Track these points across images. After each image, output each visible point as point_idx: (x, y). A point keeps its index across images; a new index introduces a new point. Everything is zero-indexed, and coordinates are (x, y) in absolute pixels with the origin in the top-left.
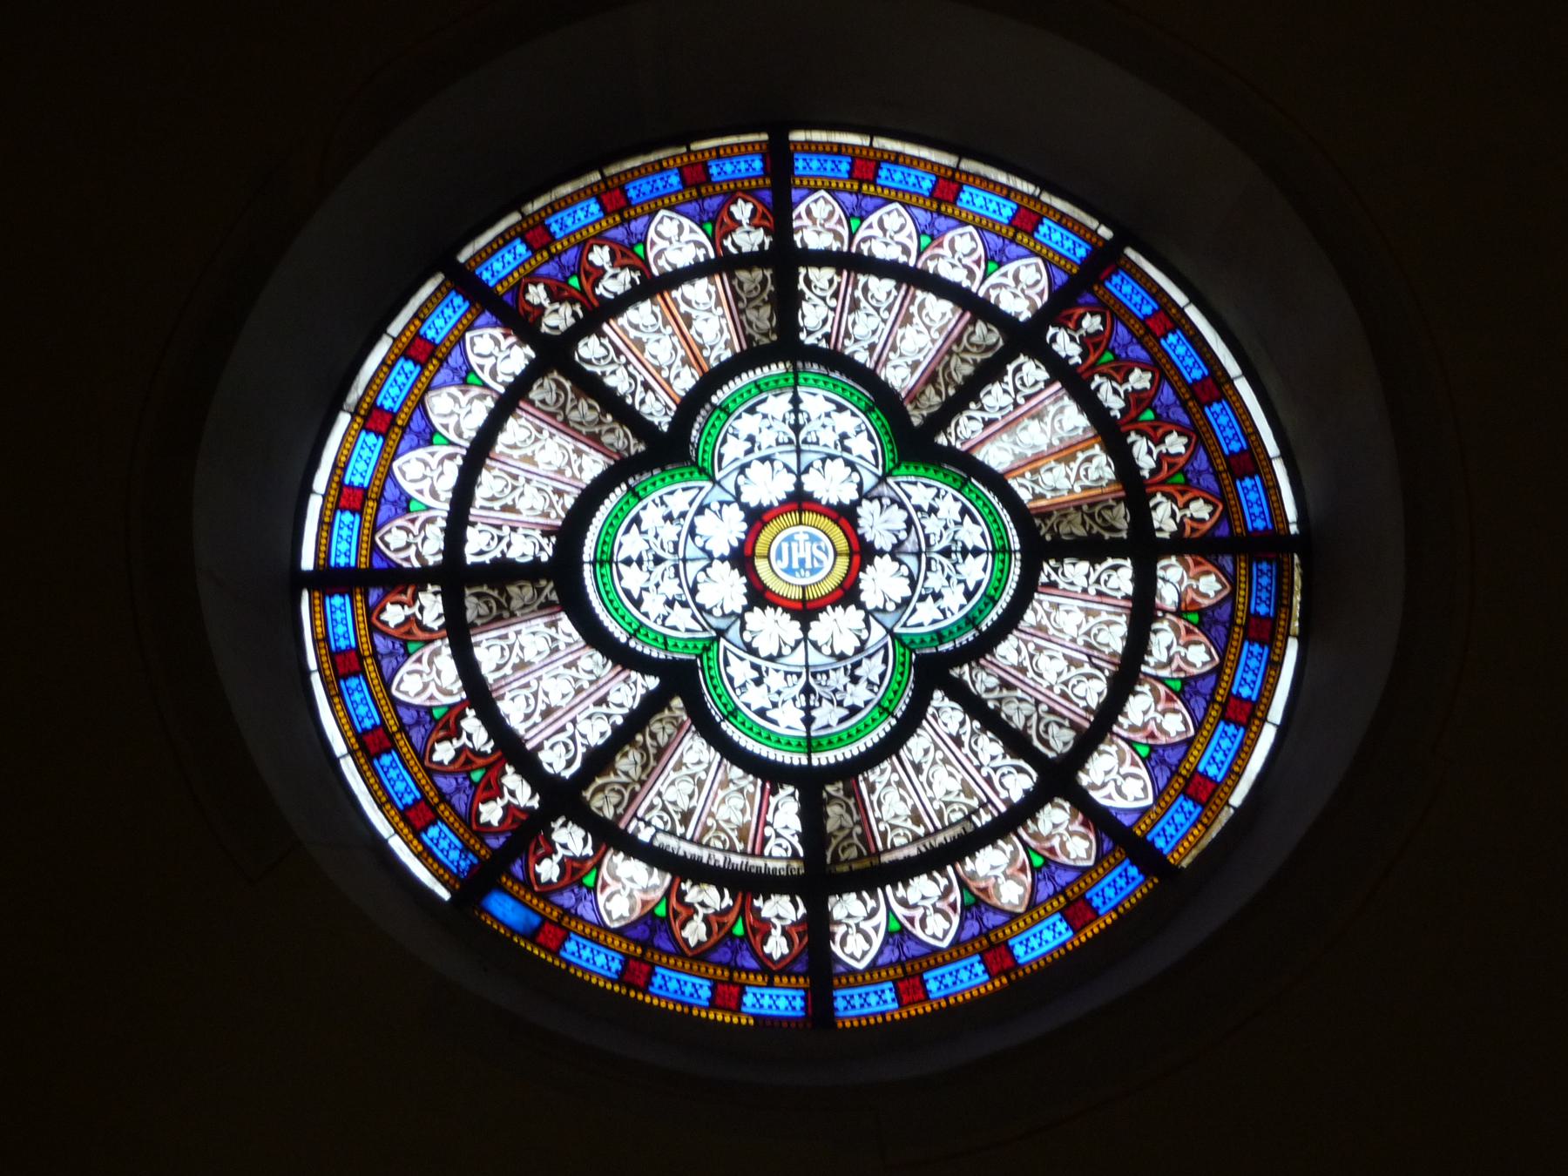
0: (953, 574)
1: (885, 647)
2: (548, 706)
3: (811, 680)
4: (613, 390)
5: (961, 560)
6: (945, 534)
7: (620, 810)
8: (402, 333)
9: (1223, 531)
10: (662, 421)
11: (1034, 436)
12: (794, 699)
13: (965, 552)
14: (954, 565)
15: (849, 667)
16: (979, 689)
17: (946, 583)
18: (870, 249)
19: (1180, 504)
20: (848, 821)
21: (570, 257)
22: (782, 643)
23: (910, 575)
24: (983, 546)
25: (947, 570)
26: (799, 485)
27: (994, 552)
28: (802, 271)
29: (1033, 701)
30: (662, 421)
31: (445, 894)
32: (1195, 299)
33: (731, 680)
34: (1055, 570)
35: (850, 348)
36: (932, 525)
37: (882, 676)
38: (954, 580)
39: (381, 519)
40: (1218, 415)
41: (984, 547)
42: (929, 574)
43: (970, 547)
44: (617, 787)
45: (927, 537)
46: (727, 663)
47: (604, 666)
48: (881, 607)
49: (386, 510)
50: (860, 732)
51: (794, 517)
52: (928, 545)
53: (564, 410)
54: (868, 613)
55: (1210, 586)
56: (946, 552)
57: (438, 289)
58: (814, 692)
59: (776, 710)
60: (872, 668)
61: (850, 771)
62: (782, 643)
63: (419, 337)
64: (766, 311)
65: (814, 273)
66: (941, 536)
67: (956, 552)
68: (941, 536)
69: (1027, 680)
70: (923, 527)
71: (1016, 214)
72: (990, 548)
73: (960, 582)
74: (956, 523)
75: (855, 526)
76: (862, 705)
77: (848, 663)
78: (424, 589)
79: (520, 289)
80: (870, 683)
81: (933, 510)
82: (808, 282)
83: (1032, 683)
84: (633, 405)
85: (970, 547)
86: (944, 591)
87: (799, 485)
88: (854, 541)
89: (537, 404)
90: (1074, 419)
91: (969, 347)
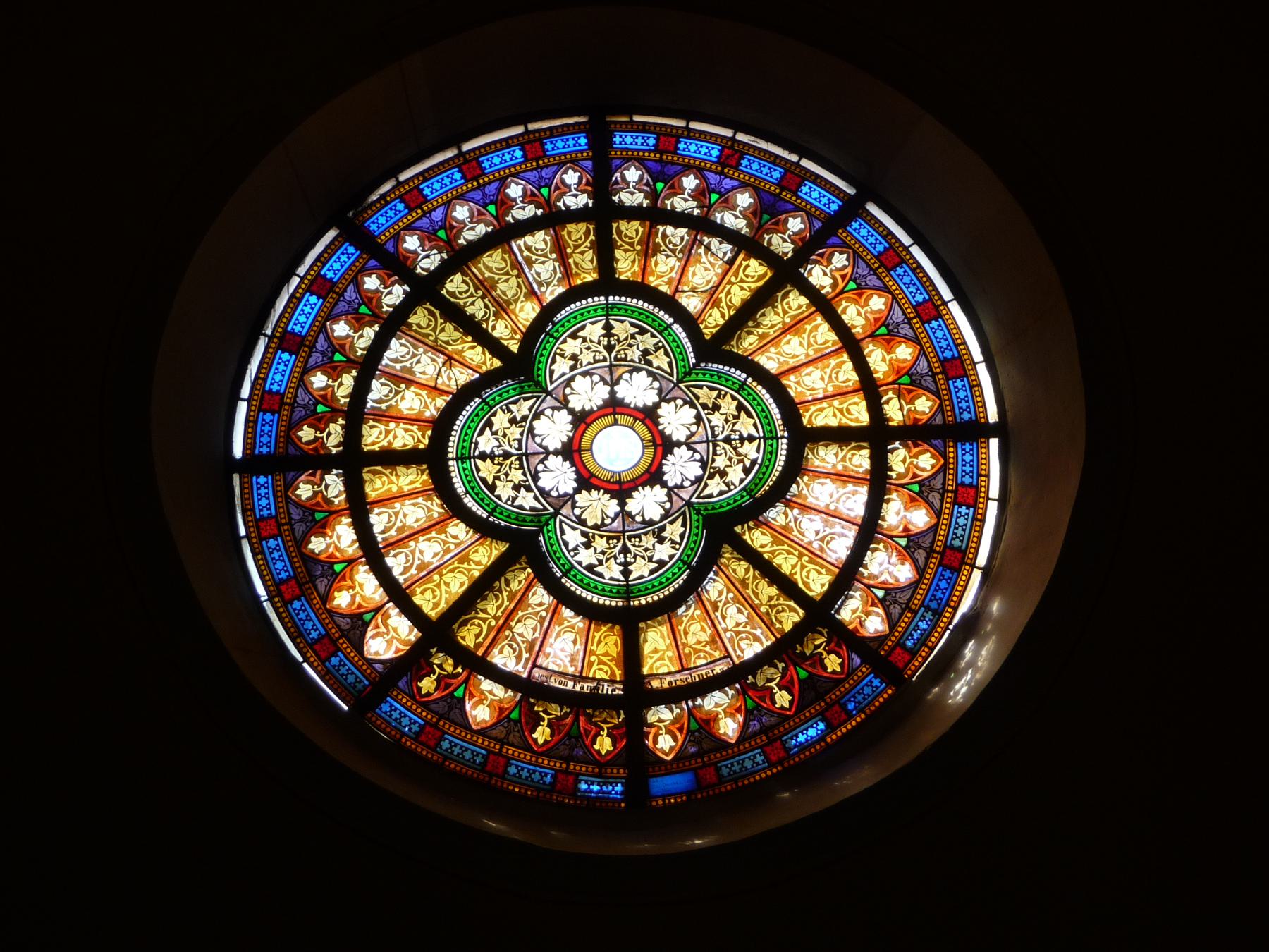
0: (501, 438)
1: (684, 513)
2: (423, 562)
3: (627, 540)
4: (770, 584)
5: (495, 449)
6: (726, 426)
7: (480, 640)
8: (308, 272)
9: (939, 420)
10: (727, 553)
11: (794, 348)
12: (616, 558)
13: (492, 457)
14: (500, 446)
15: (579, 366)
16: (756, 545)
17: (729, 463)
18: (672, 204)
19: (320, 495)
20: (577, 257)
21: (438, 215)
22: (604, 516)
23: (534, 436)
24: (755, 434)
25: (729, 453)
26: (613, 393)
27: (765, 439)
28: (615, 225)
29: (796, 553)
30: (727, 553)
31: (346, 708)
32: (919, 240)
33: (566, 544)
34: (419, 441)
35: (579, 622)
36: (517, 476)
37: (682, 536)
38: (500, 434)
39: (940, 477)
40: (282, 567)
41: (756, 435)
42: (519, 437)
43: (745, 435)
44: (749, 279)
45: (712, 428)
46: (563, 533)
47: (467, 532)
48: (556, 412)
49: (938, 483)
50: (669, 582)
51: (610, 419)
52: (714, 435)
53: (802, 565)
54: (670, 490)
55: (926, 461)
56: (727, 440)
57: (335, 239)
58: (605, 347)
59: (602, 567)
60: (674, 530)
61: (575, 294)
62: (604, 516)
63: (320, 277)
64: (590, 255)
65: (624, 225)
66: (723, 428)
67: (735, 440)
68: (723, 428)
69: (792, 537)
70: (710, 421)
71: (783, 176)
72: (762, 435)
73: (739, 462)
74: (499, 479)
75: (657, 424)
76: (667, 559)
77: (580, 370)
78: (329, 472)
79: (398, 239)
80: (673, 542)
81: (516, 488)
82: (619, 232)
83: (796, 539)
84: (754, 571)
85: (745, 435)
86: (508, 425)
87: (613, 393)
88: (576, 459)
89: (823, 571)
90: (824, 334)
91: (745, 278)
